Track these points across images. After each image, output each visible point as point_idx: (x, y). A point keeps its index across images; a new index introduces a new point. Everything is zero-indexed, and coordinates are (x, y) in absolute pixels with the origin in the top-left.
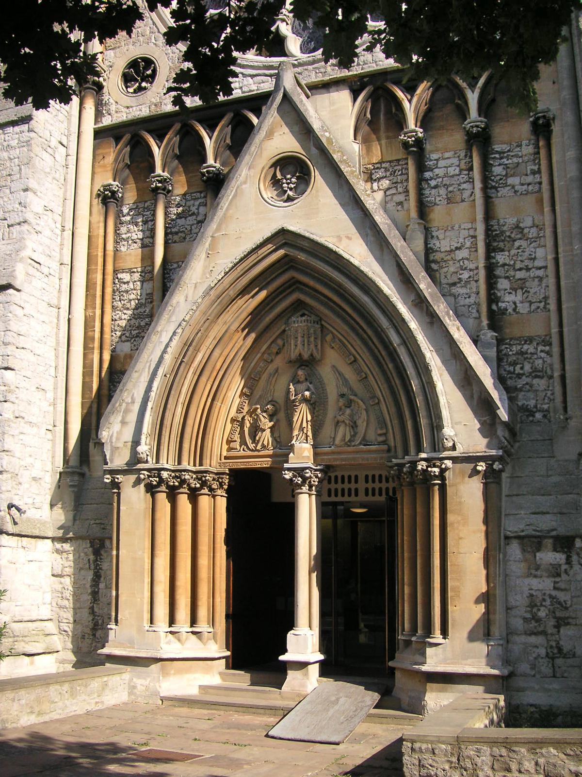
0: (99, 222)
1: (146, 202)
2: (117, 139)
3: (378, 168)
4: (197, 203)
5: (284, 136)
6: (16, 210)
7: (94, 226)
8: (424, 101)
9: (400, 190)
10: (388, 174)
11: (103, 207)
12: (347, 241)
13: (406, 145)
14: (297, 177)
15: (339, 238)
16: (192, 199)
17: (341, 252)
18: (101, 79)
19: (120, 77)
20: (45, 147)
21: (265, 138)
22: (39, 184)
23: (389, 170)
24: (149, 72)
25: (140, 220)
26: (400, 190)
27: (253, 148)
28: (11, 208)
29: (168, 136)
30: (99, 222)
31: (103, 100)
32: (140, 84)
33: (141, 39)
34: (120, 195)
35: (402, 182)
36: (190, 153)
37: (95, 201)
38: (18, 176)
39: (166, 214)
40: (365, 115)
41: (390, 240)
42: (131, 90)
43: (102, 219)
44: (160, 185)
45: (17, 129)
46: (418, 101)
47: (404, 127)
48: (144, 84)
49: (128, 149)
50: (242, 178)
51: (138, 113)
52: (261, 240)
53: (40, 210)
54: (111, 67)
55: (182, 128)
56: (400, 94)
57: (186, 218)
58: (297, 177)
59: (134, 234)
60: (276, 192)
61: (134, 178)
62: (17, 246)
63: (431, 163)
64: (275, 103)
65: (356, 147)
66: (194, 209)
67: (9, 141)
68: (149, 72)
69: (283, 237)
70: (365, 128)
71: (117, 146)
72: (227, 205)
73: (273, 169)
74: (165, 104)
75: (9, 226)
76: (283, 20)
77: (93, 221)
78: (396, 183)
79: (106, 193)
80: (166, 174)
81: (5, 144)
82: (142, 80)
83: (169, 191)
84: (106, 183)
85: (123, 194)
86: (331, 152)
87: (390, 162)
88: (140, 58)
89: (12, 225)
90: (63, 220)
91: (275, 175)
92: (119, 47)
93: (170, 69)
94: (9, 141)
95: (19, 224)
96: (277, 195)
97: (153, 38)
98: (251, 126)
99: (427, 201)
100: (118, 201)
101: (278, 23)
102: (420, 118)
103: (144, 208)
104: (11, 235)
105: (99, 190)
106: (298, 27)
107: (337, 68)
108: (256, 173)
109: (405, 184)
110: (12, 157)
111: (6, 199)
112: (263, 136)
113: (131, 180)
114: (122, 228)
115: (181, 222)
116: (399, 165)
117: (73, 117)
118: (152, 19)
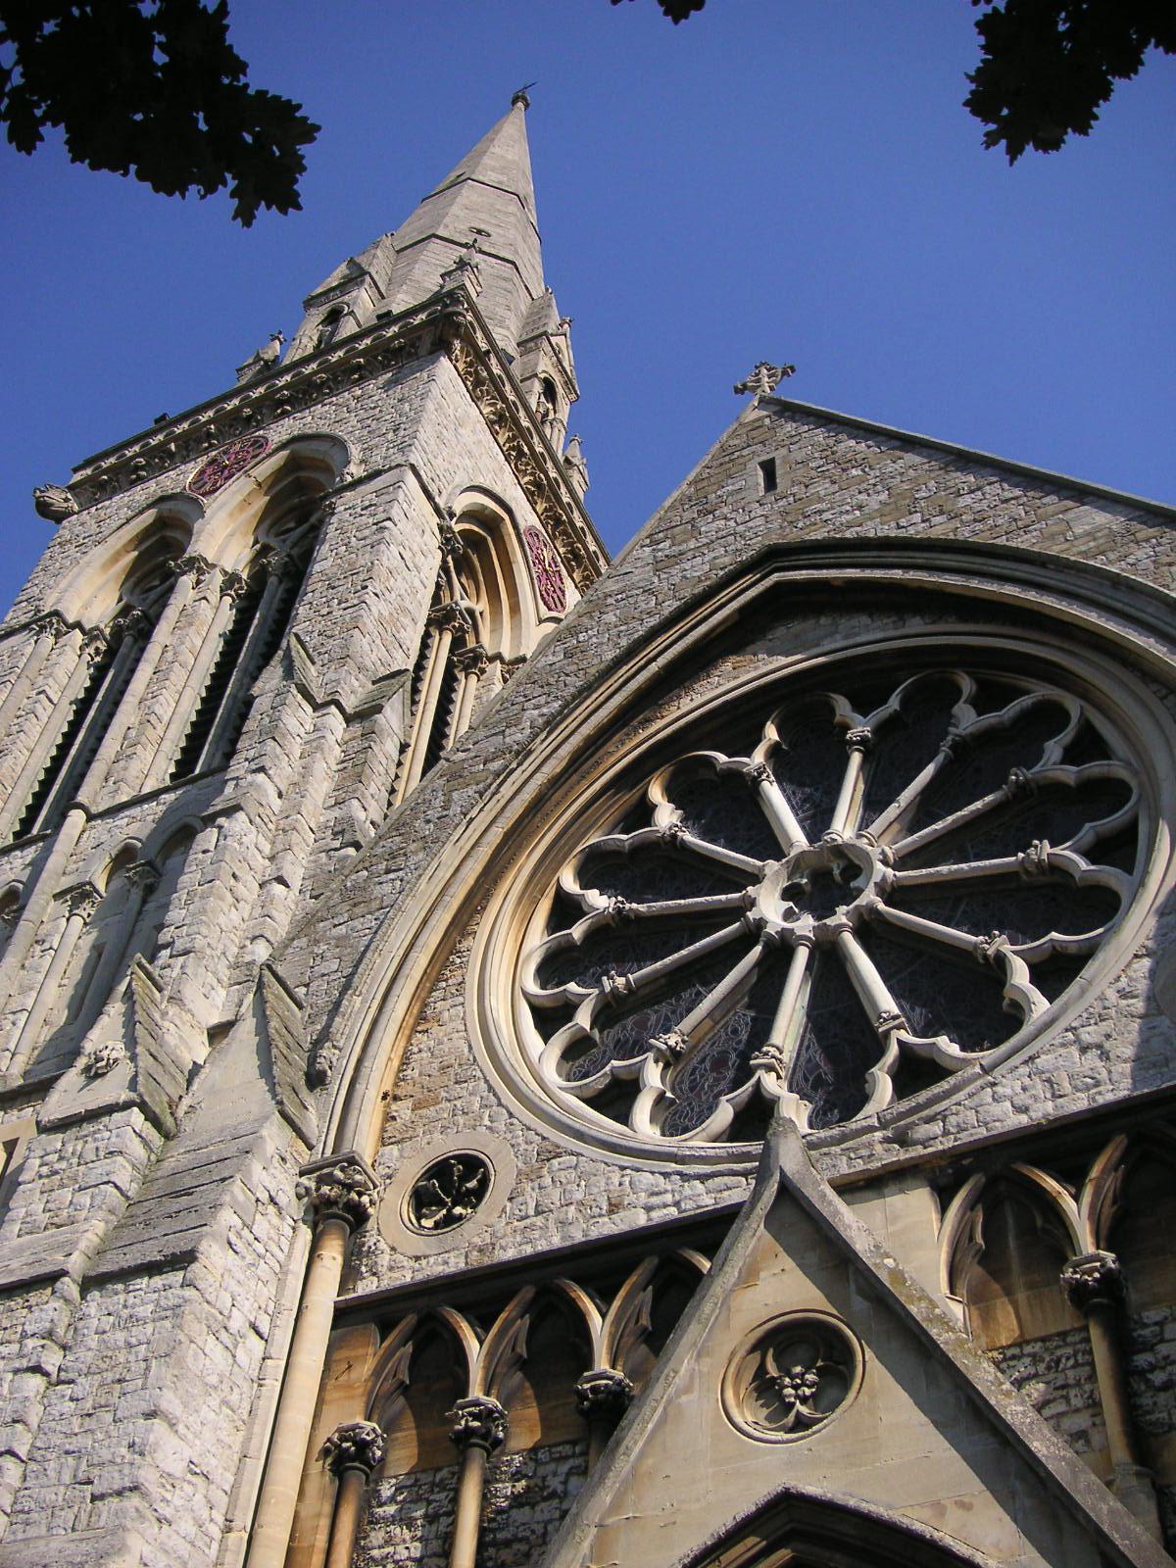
0: (319, 1515)
1: (438, 1469)
2: (385, 1330)
3: (1014, 1357)
4: (564, 1468)
5: (785, 1277)
6: (119, 1460)
7: (306, 1524)
8: (1111, 1194)
9: (1077, 1402)
10: (1041, 1367)
11: (332, 1481)
12: (960, 1512)
13: (1078, 1292)
14: (818, 1369)
15: (939, 1509)
16: (553, 1460)
17: (948, 1541)
18: (365, 1199)
19: (407, 1198)
20: (215, 1326)
21: (735, 1284)
22: (185, 1405)
23: (1042, 1360)
24: (472, 1184)
25: (419, 1513)
26: (1077, 1402)
27: (707, 1307)
28: (106, 1455)
29: (503, 1316)
30: (319, 1515)
31: (363, 1244)
32: (449, 1211)
33: (461, 1120)
34: (379, 1453)
35: (1078, 1384)
36: (553, 1351)
37: (316, 1467)
38: (140, 1382)
39: (485, 1498)
40: (971, 1238)
41: (1078, 1498)
42: (428, 1223)
43: (327, 1508)
44: (476, 1424)
45: (158, 1281)
46: (1096, 1194)
47: (1069, 1254)
48: (458, 1210)
49: (409, 1348)
50: (679, 1381)
51: (441, 1268)
52: (730, 1524)
53: (178, 1468)
54: (389, 1177)
55: (538, 1295)
56: (1051, 1184)
57: (533, 1506)
58: (818, 1369)
59: (400, 1548)
60: (765, 1411)
61: (414, 1416)
62: (102, 1545)
63: (1146, 1332)
64: (760, 1205)
65: (957, 1310)
66: (555, 1483)
67: (133, 1306)
68: (472, 1184)
69: (790, 1518)
70: (974, 1271)
71: (382, 1341)
72: (640, 1444)
73: (757, 1355)
74: (502, 1247)
75: (94, 1498)
76: (770, 1068)
77: (303, 1514)
78: (1063, 1387)
79: (345, 1445)
80: (492, 1401)
81: (125, 1313)
82: (455, 1205)
83: (497, 1443)
84: (348, 1423)
85: (385, 1452)
86: (902, 1299)
87: (1043, 1340)
88: (454, 1157)
89: (102, 1497)
90: (233, 1504)
91: (762, 1369)
92: (411, 1138)
93: (519, 1174)
94: (133, 1306)
95: (119, 1493)
96: (768, 1418)
97: (486, 1118)
98: (697, 1276)
99: (1151, 1423)
100: (371, 1467)
101: (760, 1073)
102: (1104, 1232)
103: (433, 1484)
104: (93, 1519)
105: (329, 1440)
106: (802, 1083)
107: (896, 1146)
108: (715, 1365)
109: (1087, 1387)
110: (134, 1341)
111: (100, 1436)
112: (733, 1280)
113: (409, 1421)
114: (373, 1534)
115: (521, 1515)
116: (1067, 1345)
117: (290, 1277)
118: (487, 1081)
